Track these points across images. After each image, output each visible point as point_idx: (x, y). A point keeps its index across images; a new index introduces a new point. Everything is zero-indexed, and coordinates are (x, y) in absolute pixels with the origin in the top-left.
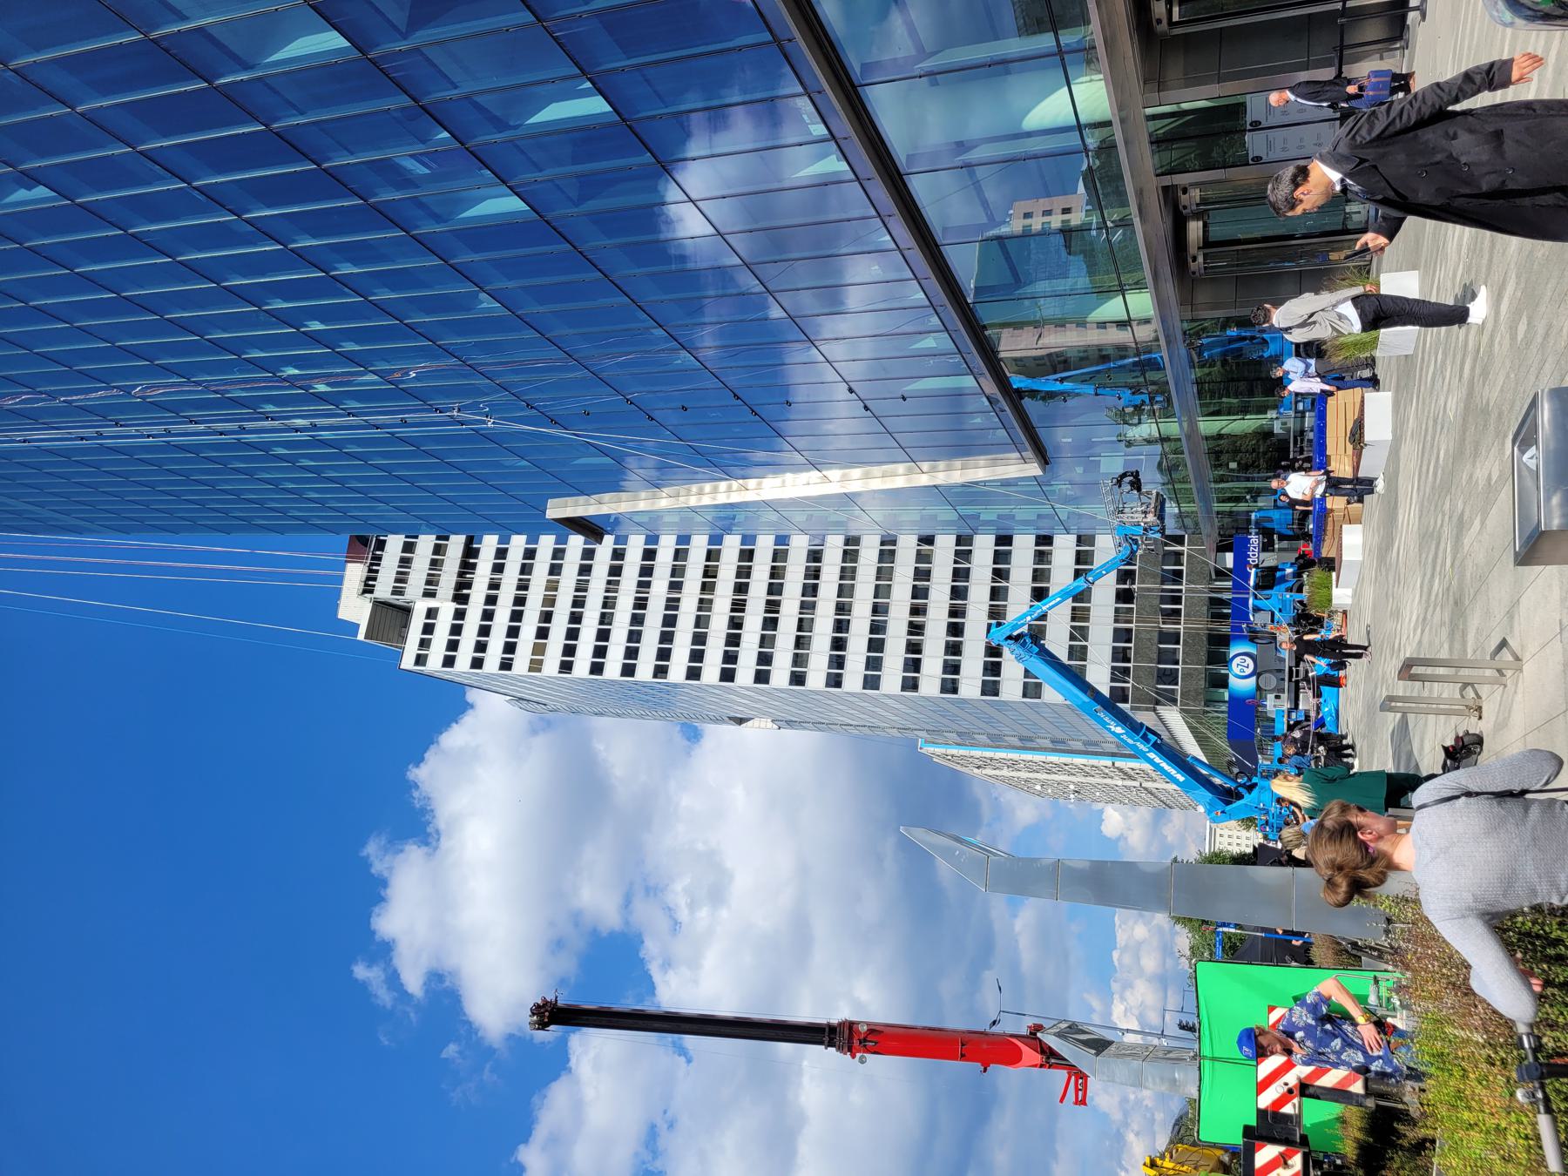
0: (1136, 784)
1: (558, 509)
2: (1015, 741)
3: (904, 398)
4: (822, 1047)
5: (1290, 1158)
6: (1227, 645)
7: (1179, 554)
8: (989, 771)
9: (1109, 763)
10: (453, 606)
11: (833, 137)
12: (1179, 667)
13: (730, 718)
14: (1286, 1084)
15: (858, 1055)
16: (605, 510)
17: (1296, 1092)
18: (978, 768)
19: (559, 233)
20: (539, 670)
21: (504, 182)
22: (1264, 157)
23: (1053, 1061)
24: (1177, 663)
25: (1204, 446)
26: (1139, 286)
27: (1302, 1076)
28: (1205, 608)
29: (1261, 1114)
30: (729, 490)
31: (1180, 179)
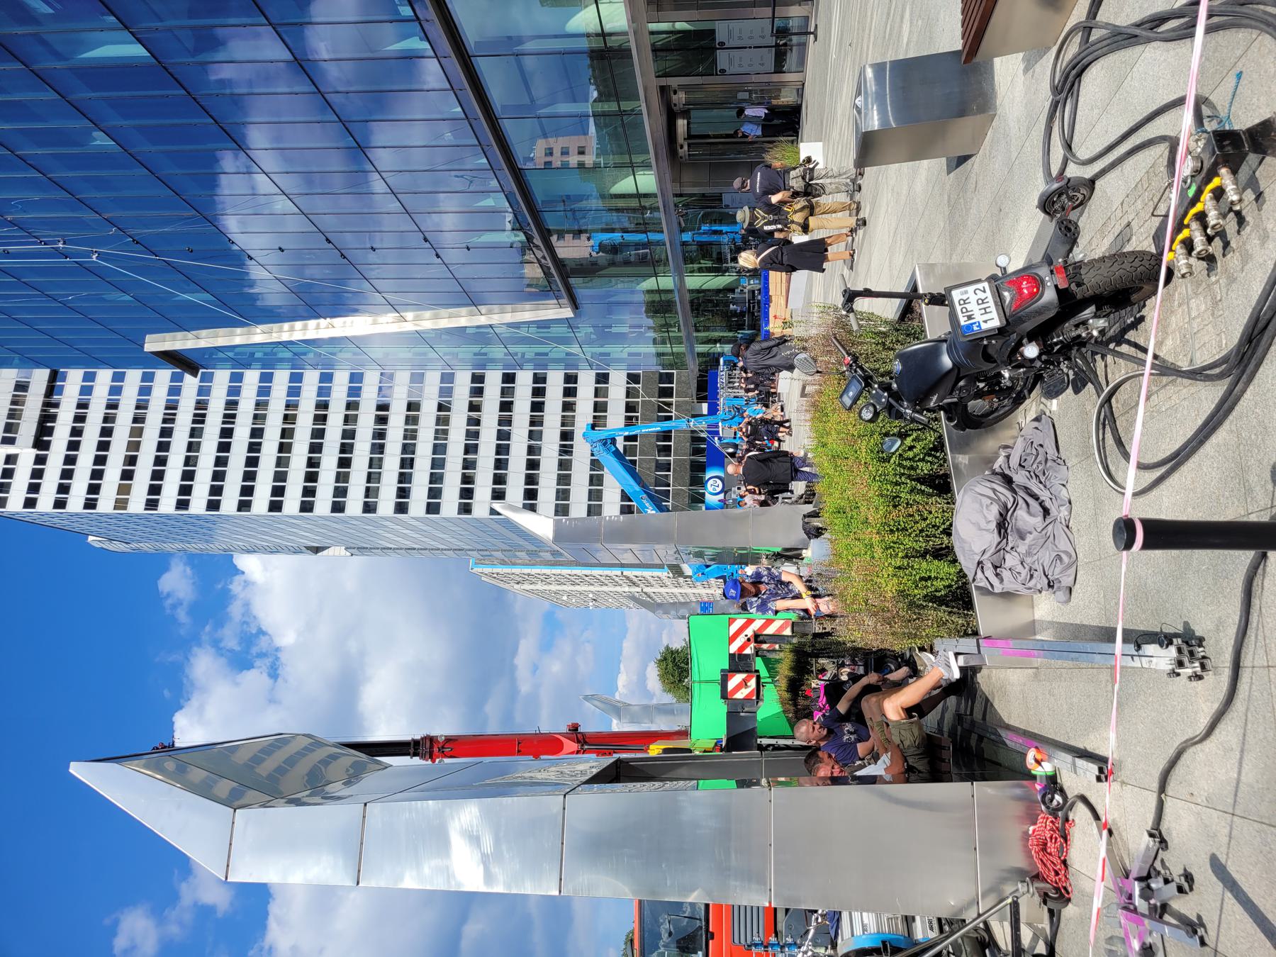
0: (639, 590)
1: (154, 343)
2: (548, 556)
3: (468, 249)
4: (409, 757)
5: (749, 681)
6: (704, 471)
7: (669, 405)
8: (527, 586)
9: (619, 573)
10: (33, 452)
11: (418, 18)
12: (670, 488)
13: (308, 548)
14: (746, 636)
15: (437, 760)
16: (203, 344)
17: (752, 640)
18: (518, 583)
19: (176, 79)
20: (125, 508)
21: (126, 27)
22: (727, 70)
23: (586, 747)
24: (669, 486)
25: (688, 297)
26: (646, 166)
27: (756, 629)
28: (688, 444)
29: (732, 656)
30: (318, 327)
31: (674, 82)
